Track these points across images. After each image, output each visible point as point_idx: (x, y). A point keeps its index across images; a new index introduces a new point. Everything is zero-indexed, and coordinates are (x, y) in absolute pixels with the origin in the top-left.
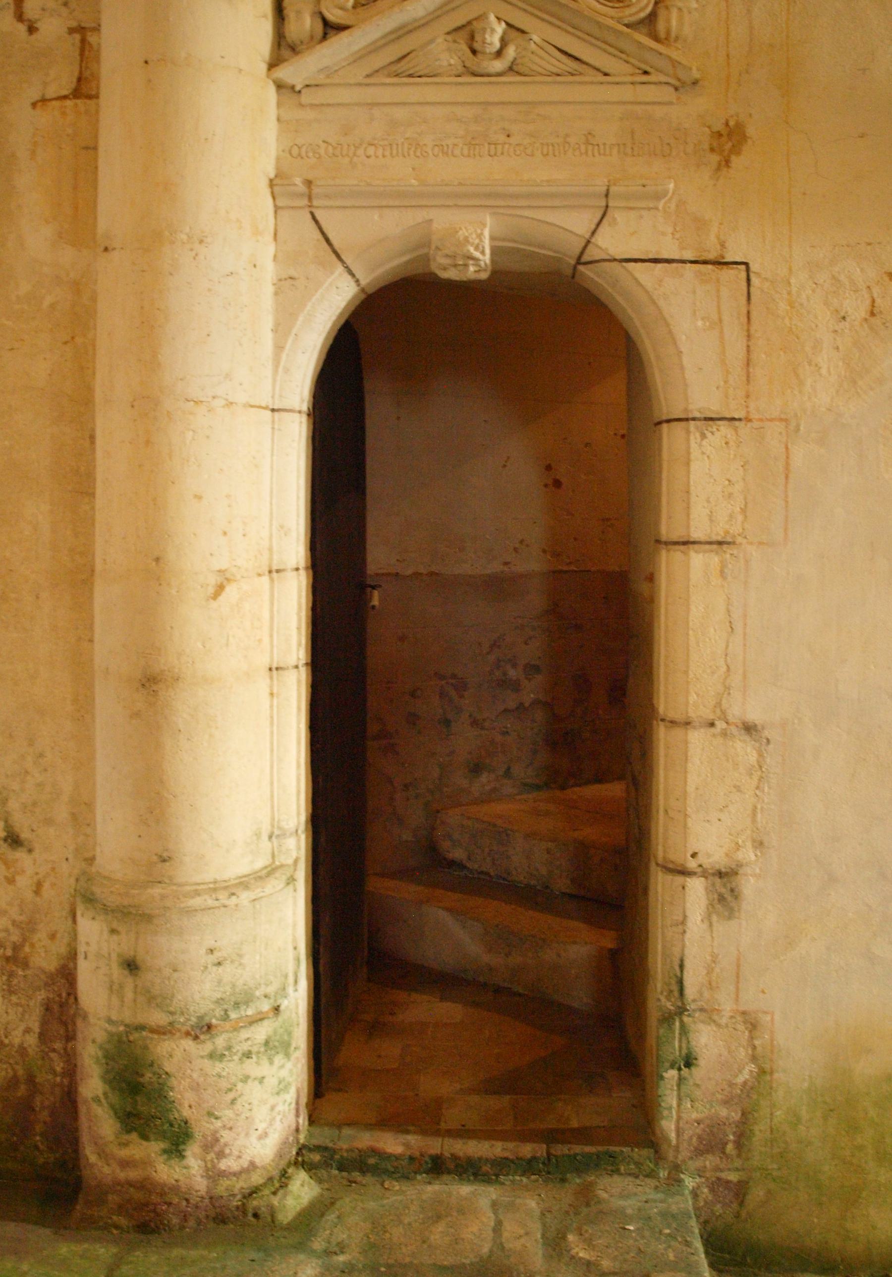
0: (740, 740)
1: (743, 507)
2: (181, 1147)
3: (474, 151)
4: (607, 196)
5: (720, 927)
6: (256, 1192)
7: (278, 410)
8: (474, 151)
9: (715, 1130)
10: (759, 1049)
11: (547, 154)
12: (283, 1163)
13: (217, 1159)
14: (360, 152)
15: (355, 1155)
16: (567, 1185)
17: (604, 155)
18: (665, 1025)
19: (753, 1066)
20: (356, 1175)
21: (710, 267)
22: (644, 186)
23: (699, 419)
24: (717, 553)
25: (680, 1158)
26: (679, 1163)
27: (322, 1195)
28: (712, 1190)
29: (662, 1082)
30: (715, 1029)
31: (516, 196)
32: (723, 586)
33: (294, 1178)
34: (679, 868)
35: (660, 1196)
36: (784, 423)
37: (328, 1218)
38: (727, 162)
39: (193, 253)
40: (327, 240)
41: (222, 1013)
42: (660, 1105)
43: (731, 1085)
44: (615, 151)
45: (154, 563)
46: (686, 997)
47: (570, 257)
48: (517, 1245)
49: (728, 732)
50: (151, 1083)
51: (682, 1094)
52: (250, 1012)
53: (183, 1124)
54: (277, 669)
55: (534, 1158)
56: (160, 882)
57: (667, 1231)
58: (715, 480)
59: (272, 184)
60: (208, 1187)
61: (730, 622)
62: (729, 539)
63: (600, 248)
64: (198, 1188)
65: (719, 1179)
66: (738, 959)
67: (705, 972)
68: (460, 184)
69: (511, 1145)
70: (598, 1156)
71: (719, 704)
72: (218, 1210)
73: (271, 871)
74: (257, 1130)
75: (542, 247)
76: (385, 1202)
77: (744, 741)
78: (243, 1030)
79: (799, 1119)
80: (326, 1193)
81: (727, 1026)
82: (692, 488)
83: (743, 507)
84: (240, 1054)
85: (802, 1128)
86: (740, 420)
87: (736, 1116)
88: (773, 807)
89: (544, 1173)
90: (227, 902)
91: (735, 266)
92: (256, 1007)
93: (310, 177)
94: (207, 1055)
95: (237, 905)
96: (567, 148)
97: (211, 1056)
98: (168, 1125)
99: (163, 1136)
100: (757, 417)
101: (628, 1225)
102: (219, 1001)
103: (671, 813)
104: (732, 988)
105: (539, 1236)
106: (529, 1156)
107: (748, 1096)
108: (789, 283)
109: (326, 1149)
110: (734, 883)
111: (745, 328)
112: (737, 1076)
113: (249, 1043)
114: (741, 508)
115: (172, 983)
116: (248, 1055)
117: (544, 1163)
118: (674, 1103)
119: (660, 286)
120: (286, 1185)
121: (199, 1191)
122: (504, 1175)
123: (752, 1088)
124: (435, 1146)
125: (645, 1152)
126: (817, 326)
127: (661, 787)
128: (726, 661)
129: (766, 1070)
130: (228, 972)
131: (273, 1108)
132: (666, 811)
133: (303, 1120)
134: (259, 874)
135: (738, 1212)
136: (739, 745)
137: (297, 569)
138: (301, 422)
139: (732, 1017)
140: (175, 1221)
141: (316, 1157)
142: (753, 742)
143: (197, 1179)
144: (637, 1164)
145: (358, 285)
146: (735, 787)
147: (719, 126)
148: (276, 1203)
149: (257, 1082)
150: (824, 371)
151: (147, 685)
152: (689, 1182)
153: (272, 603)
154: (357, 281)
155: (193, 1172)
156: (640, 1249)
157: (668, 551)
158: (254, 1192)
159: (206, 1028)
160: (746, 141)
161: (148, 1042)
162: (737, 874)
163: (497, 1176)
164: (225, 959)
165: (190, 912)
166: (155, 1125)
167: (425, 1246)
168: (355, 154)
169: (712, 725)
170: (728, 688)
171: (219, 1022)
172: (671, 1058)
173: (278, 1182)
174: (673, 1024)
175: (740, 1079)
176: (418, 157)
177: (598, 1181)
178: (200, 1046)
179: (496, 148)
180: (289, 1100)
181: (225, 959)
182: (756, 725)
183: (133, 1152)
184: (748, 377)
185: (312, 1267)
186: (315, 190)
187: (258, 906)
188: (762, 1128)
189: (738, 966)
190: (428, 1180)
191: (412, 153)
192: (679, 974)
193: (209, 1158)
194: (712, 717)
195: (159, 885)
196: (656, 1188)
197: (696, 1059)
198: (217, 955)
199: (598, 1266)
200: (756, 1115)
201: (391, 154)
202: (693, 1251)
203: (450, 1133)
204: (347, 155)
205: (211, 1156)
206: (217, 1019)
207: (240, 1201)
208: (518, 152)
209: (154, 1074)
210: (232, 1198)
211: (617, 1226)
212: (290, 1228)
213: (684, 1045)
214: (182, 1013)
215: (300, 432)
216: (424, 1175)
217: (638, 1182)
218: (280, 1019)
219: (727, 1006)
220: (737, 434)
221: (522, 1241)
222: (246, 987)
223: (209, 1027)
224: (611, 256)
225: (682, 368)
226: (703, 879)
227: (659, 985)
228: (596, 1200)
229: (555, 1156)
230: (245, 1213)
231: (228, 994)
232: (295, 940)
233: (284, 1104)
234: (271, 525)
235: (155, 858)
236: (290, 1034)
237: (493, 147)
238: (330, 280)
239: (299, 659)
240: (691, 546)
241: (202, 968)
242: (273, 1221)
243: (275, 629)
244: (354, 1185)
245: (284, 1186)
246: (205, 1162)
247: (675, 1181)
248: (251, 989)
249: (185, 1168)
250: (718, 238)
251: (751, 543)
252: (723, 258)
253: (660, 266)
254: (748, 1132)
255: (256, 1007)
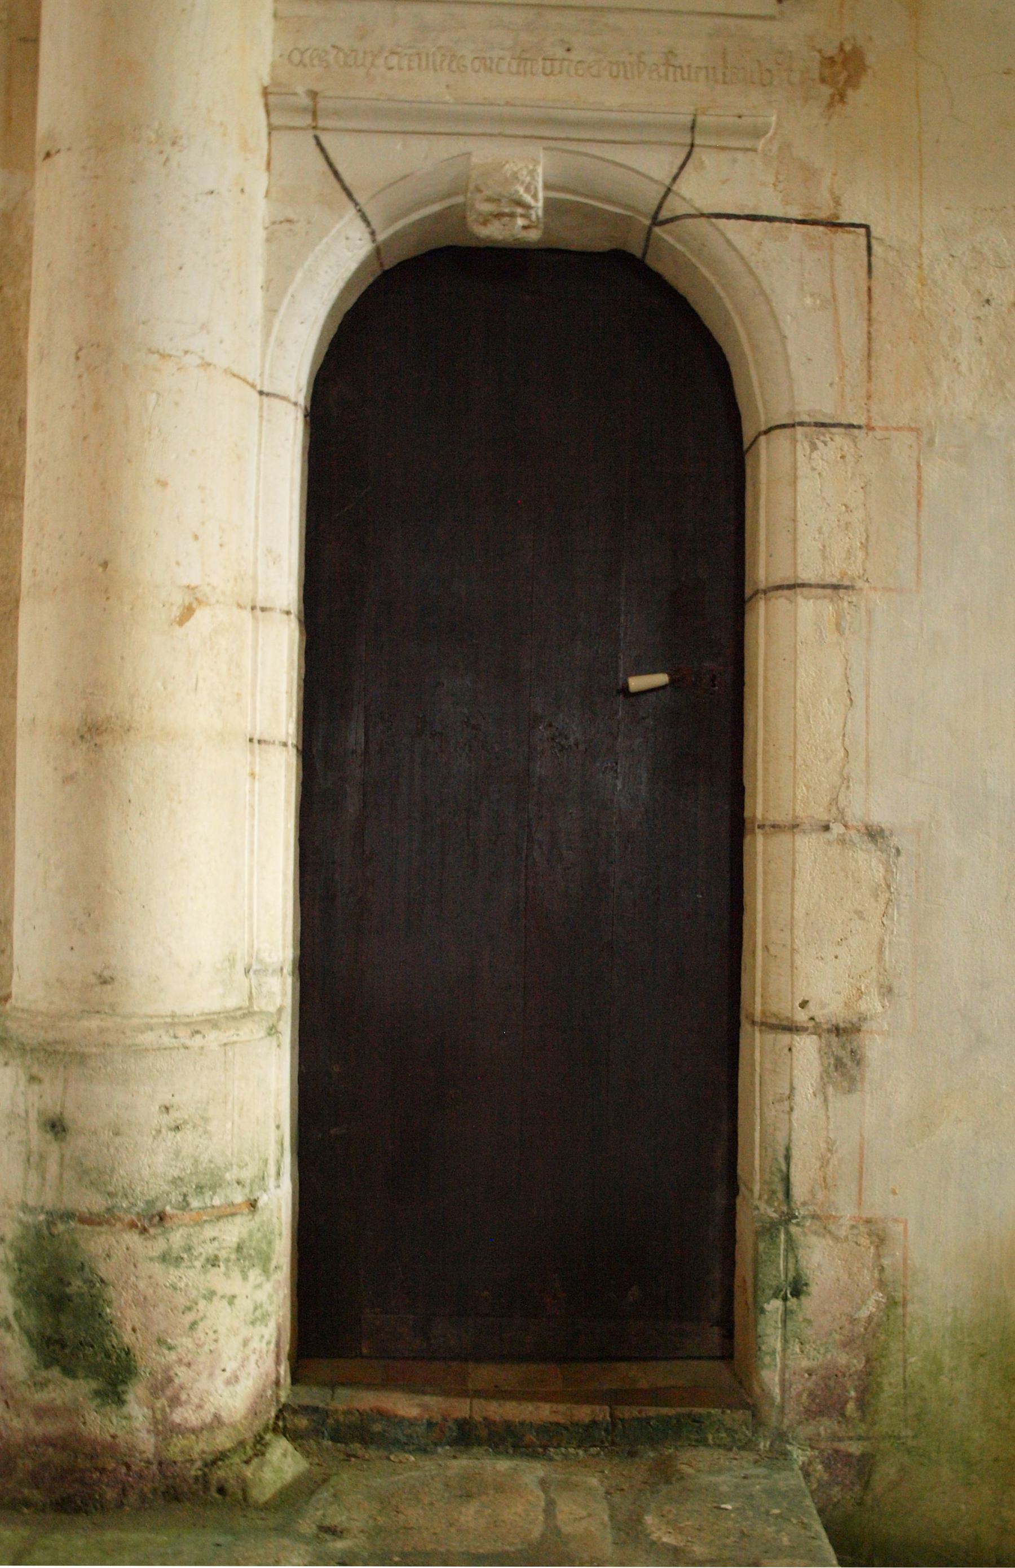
0: (861, 849)
1: (863, 541)
2: (120, 1388)
3: (525, 67)
4: (693, 128)
5: (839, 1103)
6: (220, 1459)
7: (268, 395)
8: (525, 67)
9: (832, 1383)
10: (888, 1272)
11: (616, 77)
12: (258, 1425)
13: (169, 1406)
14: (380, 61)
15: (355, 1418)
16: (637, 1459)
17: (689, 79)
18: (767, 1237)
19: (881, 1295)
20: (356, 1447)
21: (821, 228)
22: (740, 117)
23: (809, 425)
24: (832, 600)
25: (786, 1421)
26: (785, 1429)
27: (310, 1471)
28: (827, 1467)
29: (763, 1316)
30: (831, 1243)
31: (577, 124)
32: (839, 644)
33: (273, 1445)
34: (785, 1023)
35: (761, 1471)
36: (915, 434)
37: (320, 1496)
38: (842, 97)
39: (164, 157)
40: (336, 173)
41: (180, 1199)
42: (760, 1349)
43: (853, 1321)
44: (702, 74)
45: (101, 570)
46: (795, 1198)
47: (645, 215)
48: (580, 1528)
49: (847, 838)
50: (81, 1295)
51: (789, 1334)
52: (217, 1201)
53: (123, 1355)
54: (259, 742)
55: (594, 1423)
56: (98, 1012)
57: (777, 1511)
58: (829, 505)
59: (266, 93)
60: (156, 1447)
61: (849, 691)
62: (846, 582)
63: (684, 199)
64: (142, 1447)
65: (837, 1451)
66: (861, 1148)
67: (818, 1164)
68: (507, 104)
69: (562, 1407)
70: (678, 1421)
71: (835, 800)
72: (170, 1482)
73: (248, 1014)
74: (224, 1370)
75: (607, 200)
76: (396, 1478)
77: (868, 851)
78: (207, 1226)
79: (940, 1370)
80: (316, 1469)
81: (846, 1239)
82: (799, 514)
83: (863, 541)
84: (202, 1259)
85: (944, 1379)
86: (859, 427)
87: (859, 1364)
88: (904, 940)
89: (607, 1444)
90: (188, 1042)
91: (852, 229)
92: (226, 1196)
93: (315, 88)
94: (159, 1257)
95: (202, 1048)
96: (641, 69)
97: (164, 1258)
98: (103, 1355)
99: (94, 1371)
100: (880, 424)
101: (723, 1503)
102: (176, 1181)
103: (773, 949)
104: (853, 1187)
105: (606, 1518)
106: (587, 1420)
107: (874, 1336)
108: (921, 254)
109: (316, 1410)
110: (855, 1043)
111: (866, 309)
112: (859, 1309)
113: (216, 1244)
114: (862, 543)
115: (112, 1150)
116: (213, 1262)
117: (606, 1430)
118: (779, 1347)
119: (759, 250)
120: (263, 1454)
121: (144, 1452)
122: (555, 1447)
123: (879, 1325)
124: (461, 1408)
125: (740, 1415)
126: (954, 310)
127: (759, 916)
128: (843, 744)
129: (897, 1299)
130: (188, 1140)
131: (245, 1343)
132: (766, 948)
133: (284, 1369)
134: (232, 1014)
135: (862, 1498)
136: (861, 856)
137: (288, 613)
138: (297, 418)
139: (853, 1227)
140: (110, 1494)
141: (303, 1422)
142: (879, 853)
143: (141, 1435)
144: (730, 1431)
145: (374, 241)
146: (856, 912)
147: (831, 51)
148: (249, 1474)
149: (225, 1302)
150: (964, 368)
151: (88, 736)
152: (799, 1455)
153: (255, 653)
154: (373, 233)
155: (137, 1424)
156: (742, 1532)
157: (767, 600)
158: (222, 1456)
159: (157, 1218)
160: (865, 71)
161: (77, 1236)
162: (859, 1030)
163: (545, 1447)
164: (185, 1122)
165: (139, 1052)
166: (84, 1355)
167: (453, 1530)
168: (372, 64)
169: (827, 828)
170: (846, 779)
171: (175, 1211)
172: (774, 1283)
173: (251, 1448)
174: (777, 1236)
175: (864, 1314)
176: (453, 72)
177: (678, 1454)
178: (149, 1244)
179: (552, 65)
180: (267, 1337)
181: (185, 1122)
182: (882, 831)
183: (53, 1395)
184: (869, 372)
185: (300, 1554)
186: (322, 104)
187: (230, 1054)
188: (892, 1381)
189: (862, 1156)
190: (452, 1455)
191: (445, 64)
192: (784, 1167)
193: (158, 1405)
194: (826, 818)
195: (97, 1015)
196: (756, 1462)
197: (806, 1284)
198: (174, 1114)
199: (689, 1552)
200: (884, 1362)
201: (419, 66)
202: (813, 1535)
203: (478, 1394)
204: (363, 65)
205: (161, 1402)
206: (173, 1207)
207: (200, 1469)
208: (580, 72)
209: (85, 1281)
210: (188, 1465)
211: (710, 1505)
212: (267, 1507)
213: (791, 1266)
214: (126, 1196)
215: (295, 430)
216: (448, 1447)
217: (731, 1455)
218: (257, 1218)
219: (847, 1212)
220: (856, 445)
221: (584, 1524)
222: (212, 1166)
223: (162, 1217)
224: (696, 209)
225: (787, 359)
226: (815, 1037)
227: (757, 1188)
228: (678, 1476)
229: (622, 1420)
230: (206, 1488)
231: (188, 1172)
232: (278, 1115)
233: (261, 1341)
234: (256, 547)
235: (92, 979)
236: (270, 1243)
237: (548, 63)
238: (338, 226)
239: (287, 733)
240: (798, 590)
241: (154, 1132)
242: (245, 1499)
243: (258, 688)
244: (353, 1459)
245: (260, 1454)
246: (153, 1410)
247: (778, 1457)
248: (219, 1168)
249: (125, 1418)
250: (831, 192)
251: (875, 589)
252: (838, 218)
253: (758, 225)
254: (875, 1386)
255: (226, 1196)
